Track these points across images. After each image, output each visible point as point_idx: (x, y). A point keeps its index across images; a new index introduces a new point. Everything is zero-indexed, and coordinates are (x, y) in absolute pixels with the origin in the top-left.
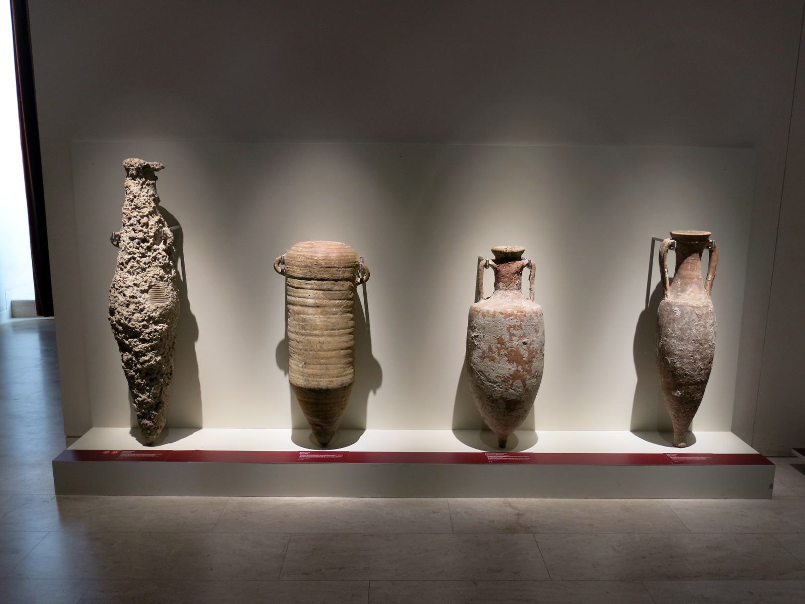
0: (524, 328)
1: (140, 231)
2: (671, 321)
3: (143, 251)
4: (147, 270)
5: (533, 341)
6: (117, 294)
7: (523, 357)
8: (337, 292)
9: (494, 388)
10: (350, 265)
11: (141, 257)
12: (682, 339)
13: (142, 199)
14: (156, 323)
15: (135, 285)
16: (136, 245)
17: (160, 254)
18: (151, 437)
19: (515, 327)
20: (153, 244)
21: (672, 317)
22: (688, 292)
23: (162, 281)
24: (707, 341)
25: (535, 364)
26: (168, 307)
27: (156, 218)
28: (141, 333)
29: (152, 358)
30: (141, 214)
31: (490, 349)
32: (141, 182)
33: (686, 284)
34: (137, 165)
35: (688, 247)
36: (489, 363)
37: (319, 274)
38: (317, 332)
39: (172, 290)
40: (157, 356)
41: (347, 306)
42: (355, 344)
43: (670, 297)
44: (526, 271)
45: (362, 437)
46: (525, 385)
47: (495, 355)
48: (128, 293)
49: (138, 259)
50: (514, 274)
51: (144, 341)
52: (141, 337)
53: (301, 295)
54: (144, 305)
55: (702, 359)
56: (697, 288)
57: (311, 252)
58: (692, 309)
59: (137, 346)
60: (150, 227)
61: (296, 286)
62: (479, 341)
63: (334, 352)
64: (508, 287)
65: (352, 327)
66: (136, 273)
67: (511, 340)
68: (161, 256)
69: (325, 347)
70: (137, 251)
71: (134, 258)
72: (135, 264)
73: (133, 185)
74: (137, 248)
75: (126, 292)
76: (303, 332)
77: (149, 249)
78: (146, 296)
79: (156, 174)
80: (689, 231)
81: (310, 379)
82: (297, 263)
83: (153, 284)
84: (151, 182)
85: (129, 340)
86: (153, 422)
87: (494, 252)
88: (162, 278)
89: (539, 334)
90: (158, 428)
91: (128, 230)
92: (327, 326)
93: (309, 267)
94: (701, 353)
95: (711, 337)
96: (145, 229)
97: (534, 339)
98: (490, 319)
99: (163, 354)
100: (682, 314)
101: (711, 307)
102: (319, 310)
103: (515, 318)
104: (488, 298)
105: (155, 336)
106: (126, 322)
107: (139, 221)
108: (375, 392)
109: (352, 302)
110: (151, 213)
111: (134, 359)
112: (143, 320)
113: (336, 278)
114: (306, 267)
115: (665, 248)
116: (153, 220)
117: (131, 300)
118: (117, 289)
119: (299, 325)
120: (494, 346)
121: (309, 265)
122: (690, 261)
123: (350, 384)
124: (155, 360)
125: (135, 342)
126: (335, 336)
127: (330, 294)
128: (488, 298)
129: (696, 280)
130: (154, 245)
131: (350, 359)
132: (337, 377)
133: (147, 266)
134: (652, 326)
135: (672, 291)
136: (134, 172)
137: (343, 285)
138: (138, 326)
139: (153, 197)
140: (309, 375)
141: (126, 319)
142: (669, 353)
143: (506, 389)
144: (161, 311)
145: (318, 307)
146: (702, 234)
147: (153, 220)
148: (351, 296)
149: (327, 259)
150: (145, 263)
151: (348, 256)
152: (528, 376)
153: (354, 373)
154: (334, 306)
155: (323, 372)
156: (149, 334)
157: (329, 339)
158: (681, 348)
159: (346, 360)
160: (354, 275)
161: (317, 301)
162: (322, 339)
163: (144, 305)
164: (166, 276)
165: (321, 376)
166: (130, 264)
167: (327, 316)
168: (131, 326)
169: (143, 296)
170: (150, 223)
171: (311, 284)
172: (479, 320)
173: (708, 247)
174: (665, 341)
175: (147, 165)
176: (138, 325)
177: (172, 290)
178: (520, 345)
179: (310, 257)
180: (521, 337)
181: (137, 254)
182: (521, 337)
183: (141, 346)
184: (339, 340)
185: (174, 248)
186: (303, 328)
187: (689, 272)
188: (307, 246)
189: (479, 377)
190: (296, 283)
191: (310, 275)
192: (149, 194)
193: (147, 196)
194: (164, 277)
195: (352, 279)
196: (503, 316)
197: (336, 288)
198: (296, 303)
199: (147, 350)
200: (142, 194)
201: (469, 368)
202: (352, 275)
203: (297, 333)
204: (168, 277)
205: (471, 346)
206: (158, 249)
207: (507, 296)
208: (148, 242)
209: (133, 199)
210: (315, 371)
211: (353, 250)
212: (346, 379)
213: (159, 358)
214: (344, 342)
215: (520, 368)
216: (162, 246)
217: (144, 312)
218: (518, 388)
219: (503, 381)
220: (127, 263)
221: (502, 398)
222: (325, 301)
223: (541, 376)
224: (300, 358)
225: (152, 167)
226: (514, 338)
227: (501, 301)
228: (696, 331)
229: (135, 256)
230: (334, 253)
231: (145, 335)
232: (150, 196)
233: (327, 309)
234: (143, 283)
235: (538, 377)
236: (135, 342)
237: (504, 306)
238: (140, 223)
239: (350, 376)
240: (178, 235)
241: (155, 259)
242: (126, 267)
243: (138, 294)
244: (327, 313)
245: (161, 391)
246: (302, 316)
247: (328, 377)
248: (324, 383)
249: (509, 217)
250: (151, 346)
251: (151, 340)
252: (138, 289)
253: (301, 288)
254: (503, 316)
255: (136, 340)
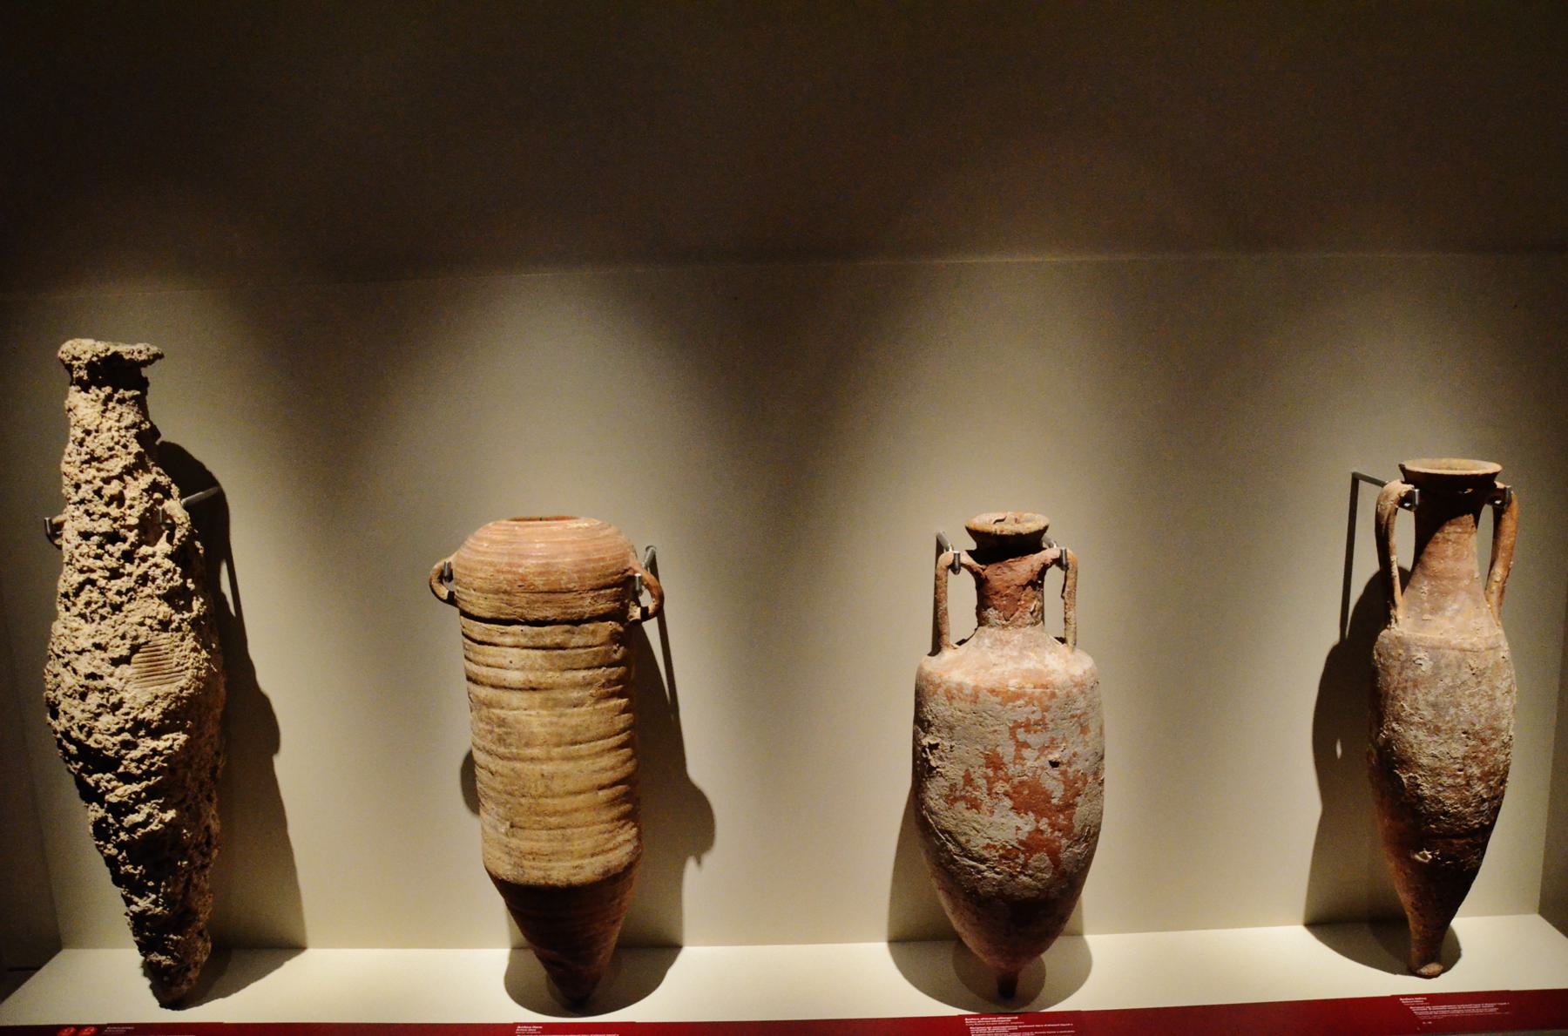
0: (1051, 726)
1: (103, 515)
2: (1409, 684)
3: (113, 563)
4: (126, 607)
5: (1075, 755)
6: (59, 669)
7: (1049, 797)
8: (581, 651)
9: (980, 872)
10: (609, 580)
11: (109, 579)
12: (1437, 730)
13: (104, 437)
14: (156, 734)
15: (97, 646)
16: (94, 550)
17: (157, 566)
18: (174, 989)
19: (1028, 726)
20: (136, 546)
21: (1410, 673)
22: (1448, 614)
23: (165, 630)
24: (1496, 731)
25: (1082, 810)
26: (185, 694)
27: (145, 480)
28: (118, 760)
29: (154, 817)
30: (104, 474)
31: (968, 780)
32: (102, 396)
33: (1445, 594)
34: (88, 356)
35: (1442, 502)
36: (967, 814)
37: (534, 610)
38: (535, 752)
39: (194, 650)
40: (163, 809)
41: (609, 683)
42: (637, 767)
43: (1404, 624)
44: (1054, 576)
45: (672, 973)
46: (1056, 862)
47: (981, 794)
48: (84, 665)
49: (102, 583)
50: (1024, 587)
51: (127, 778)
52: (121, 769)
53: (490, 661)
54: (122, 694)
55: (1485, 777)
56: (1468, 602)
57: (509, 554)
58: (1460, 656)
59: (113, 790)
60: (128, 503)
61: (479, 638)
62: (941, 758)
63: (581, 797)
64: (1008, 619)
65: (623, 730)
66: (97, 617)
67: (1019, 758)
68: (158, 572)
69: (556, 786)
70: (99, 563)
71: (93, 582)
72: (95, 595)
73: (82, 404)
74: (98, 557)
75: (76, 665)
76: (502, 750)
77: (128, 556)
78: (125, 670)
79: (145, 372)
80: (1425, 461)
81: (526, 863)
82: (477, 583)
83: (142, 640)
84: (128, 394)
85: (95, 776)
86: (173, 958)
87: (974, 533)
88: (165, 625)
89: (1092, 734)
90: (188, 969)
91: (77, 513)
92: (560, 735)
93: (505, 592)
94: (1482, 762)
95: (1505, 722)
96: (114, 511)
97: (1079, 749)
98: (966, 706)
99: (183, 801)
100: (1436, 668)
101: (1505, 650)
102: (538, 696)
103: (1027, 704)
104: (960, 643)
105: (153, 764)
106: (82, 737)
107: (98, 492)
108: (699, 862)
109: (620, 670)
110: (129, 470)
111: (111, 820)
112: (121, 731)
113: (575, 617)
114: (497, 592)
115: (1389, 505)
116: (135, 488)
117: (91, 683)
118: (59, 656)
119: (491, 732)
120: (978, 774)
121: (505, 587)
122: (1452, 537)
123: (629, 867)
124: (161, 821)
125: (109, 781)
126: (581, 757)
127: (561, 656)
128: (960, 643)
129: (1466, 582)
130: (140, 546)
131: (626, 807)
132: (593, 855)
133: (125, 599)
134: (1356, 688)
135: (1408, 609)
136: (83, 374)
137: (594, 633)
138: (109, 745)
139: (134, 431)
140: (523, 855)
141: (81, 728)
142: (1404, 762)
143: (1011, 875)
144: (165, 705)
145: (534, 689)
146: (1481, 472)
147: (135, 488)
148: (617, 656)
149: (549, 573)
150: (119, 593)
151: (603, 559)
152: (1064, 841)
153: (639, 837)
154: (576, 685)
155: (556, 846)
156: (141, 760)
157: (567, 767)
158: (1432, 753)
159: (615, 812)
160: (623, 604)
161: (531, 677)
162: (548, 768)
163: (122, 694)
164: (177, 617)
165: (552, 856)
166: (84, 597)
167: (558, 710)
168: (94, 745)
169: (118, 671)
170: (128, 494)
171: (514, 634)
172: (938, 708)
173: (1491, 502)
174: (1393, 730)
175: (115, 354)
176: (110, 743)
177: (194, 650)
178: (1043, 768)
179: (506, 568)
180: (1044, 749)
181: (100, 573)
182: (1044, 749)
183: (123, 791)
184: (591, 768)
185: (198, 544)
186: (501, 740)
187: (1450, 564)
188: (499, 538)
189: (944, 845)
190: (478, 629)
191: (508, 612)
192: (123, 424)
193: (119, 429)
194: (171, 622)
195: (619, 615)
196: (998, 699)
197: (577, 640)
198: (480, 678)
199: (138, 799)
200: (105, 426)
201: (919, 820)
202: (617, 604)
203: (490, 753)
204: (183, 620)
205: (922, 771)
206: (153, 556)
207: (1008, 642)
208: (124, 540)
209: (83, 440)
210: (535, 846)
211: (622, 539)
212: (618, 857)
213: (171, 814)
214: (605, 770)
215: (1044, 824)
216: (163, 546)
217: (123, 710)
218: (1041, 871)
219: (1001, 856)
220: (77, 595)
221: (1001, 894)
222: (550, 674)
223: (1096, 834)
224: (501, 811)
225: (127, 357)
226: (1026, 753)
227: (992, 657)
228: (1469, 710)
229: (94, 576)
230: (566, 554)
231: (129, 766)
232: (127, 428)
233: (557, 694)
234: (118, 641)
235: (1090, 837)
236: (109, 781)
237: (998, 670)
238: (101, 497)
239: (629, 848)
240: (211, 517)
241: (144, 579)
242: (74, 604)
243: (106, 668)
244: (557, 703)
245: (186, 888)
246: (497, 711)
247: (578, 854)
248: (561, 872)
249: (996, 428)
250: (146, 789)
251: (147, 775)
252: (104, 655)
253: (490, 644)
254: (998, 699)
255: (109, 776)
